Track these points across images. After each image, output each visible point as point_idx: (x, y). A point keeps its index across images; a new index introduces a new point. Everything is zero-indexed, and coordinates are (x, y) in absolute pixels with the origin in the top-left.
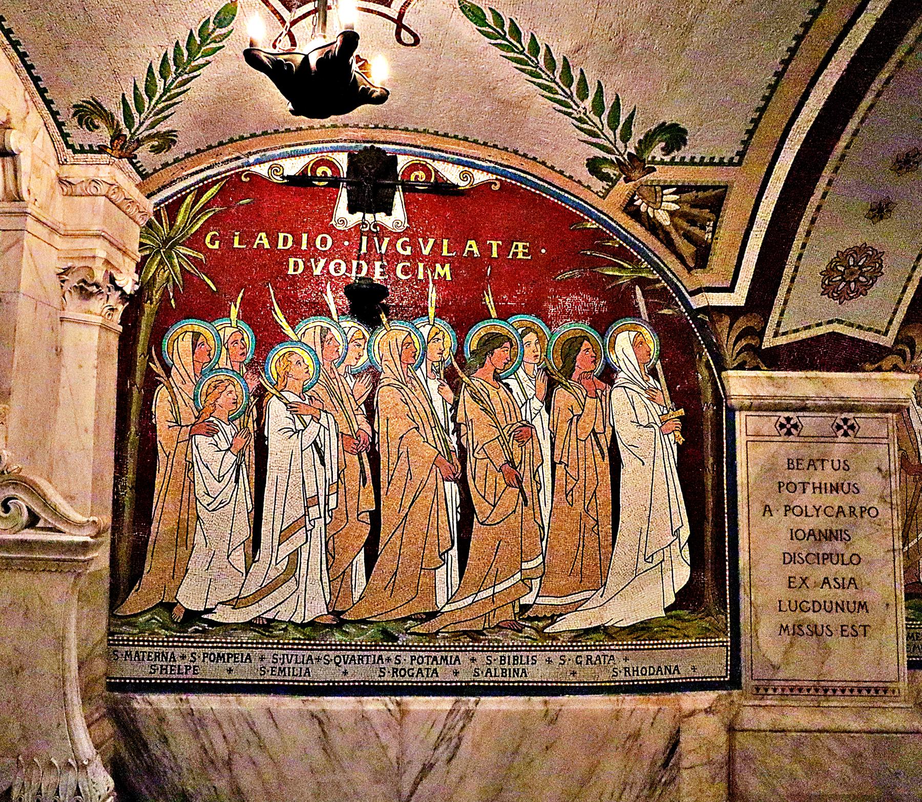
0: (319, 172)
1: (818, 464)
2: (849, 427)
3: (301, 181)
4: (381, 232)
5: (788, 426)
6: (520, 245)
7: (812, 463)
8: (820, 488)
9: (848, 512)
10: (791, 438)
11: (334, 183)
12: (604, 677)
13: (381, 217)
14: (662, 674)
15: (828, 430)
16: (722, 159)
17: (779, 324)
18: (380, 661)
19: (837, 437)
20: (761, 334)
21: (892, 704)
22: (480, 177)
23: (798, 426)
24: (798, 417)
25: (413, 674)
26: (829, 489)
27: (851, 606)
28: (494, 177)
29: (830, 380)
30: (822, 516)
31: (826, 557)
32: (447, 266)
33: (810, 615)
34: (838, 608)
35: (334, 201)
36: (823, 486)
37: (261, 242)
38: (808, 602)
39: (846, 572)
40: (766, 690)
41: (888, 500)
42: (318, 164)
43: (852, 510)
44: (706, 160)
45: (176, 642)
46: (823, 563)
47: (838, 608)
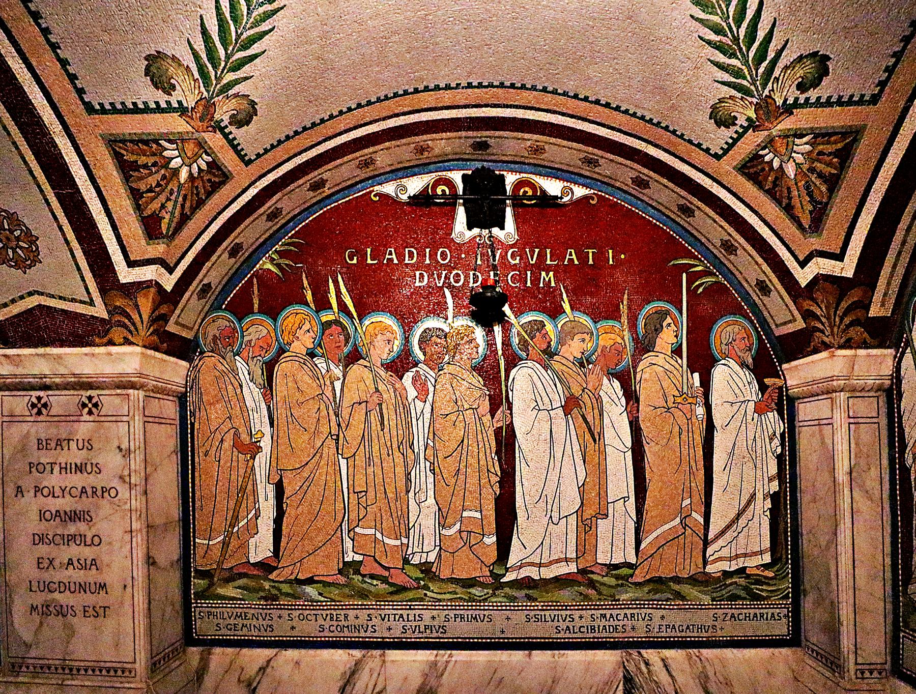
1: (65, 444)
4: (494, 244)
5: (39, 406)
7: (59, 443)
8: (66, 468)
9: (91, 493)
10: (41, 418)
13: (496, 231)
15: (73, 409)
17: (81, 302)
21: (127, 685)
23: (98, 405)
24: (47, 396)
25: (683, 630)
26: (73, 470)
27: (93, 587)
28: (592, 191)
29: (59, 357)
30: (67, 496)
31: (70, 538)
32: (551, 274)
33: (56, 595)
34: (81, 590)
35: (452, 217)
36: (68, 467)
37: (390, 257)
38: (55, 583)
39: (88, 553)
40: (21, 667)
41: (127, 479)
42: (437, 183)
43: (94, 490)
46: (68, 545)
47: (81, 590)
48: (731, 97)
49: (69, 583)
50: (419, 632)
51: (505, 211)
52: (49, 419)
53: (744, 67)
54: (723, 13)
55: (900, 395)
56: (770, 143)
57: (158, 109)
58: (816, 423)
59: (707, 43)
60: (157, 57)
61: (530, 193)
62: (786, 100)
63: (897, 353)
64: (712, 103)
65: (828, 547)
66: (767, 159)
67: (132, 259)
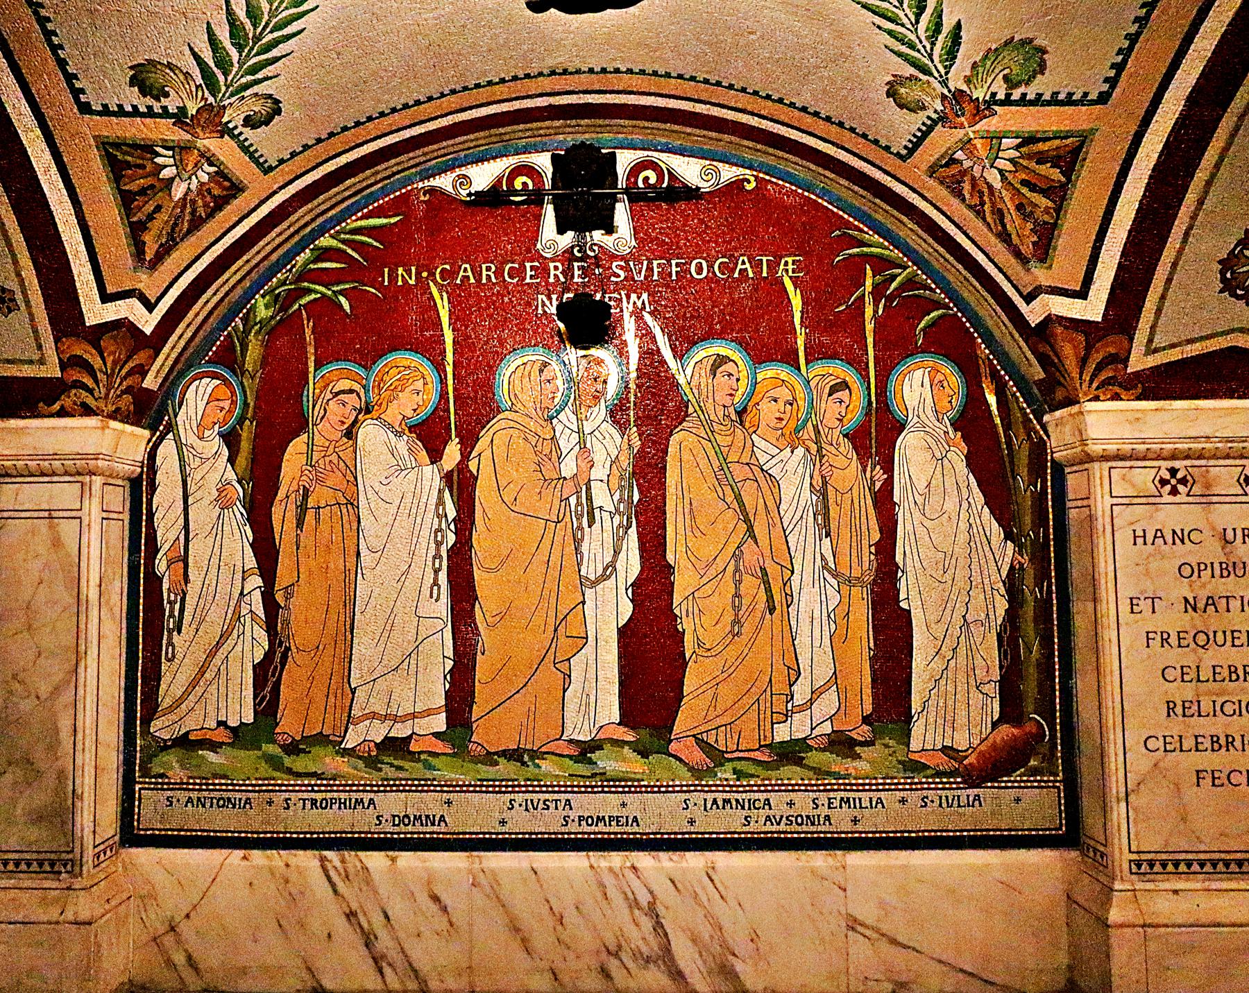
0: (518, 184)
2: (1168, 482)
5: (1173, 482)
6: (790, 260)
10: (1178, 499)
11: (536, 198)
12: (759, 826)
14: (422, 825)
18: (248, 806)
20: (1126, 361)
35: (538, 217)
44: (1047, 97)
45: (491, 786)
48: (187, 75)
52: (1191, 499)
53: (237, 65)
54: (277, 9)
55: (153, 488)
56: (181, 150)
58: (46, 514)
59: (227, 9)
62: (230, 122)
63: (153, 436)
64: (155, 57)
65: (56, 691)
66: (159, 160)
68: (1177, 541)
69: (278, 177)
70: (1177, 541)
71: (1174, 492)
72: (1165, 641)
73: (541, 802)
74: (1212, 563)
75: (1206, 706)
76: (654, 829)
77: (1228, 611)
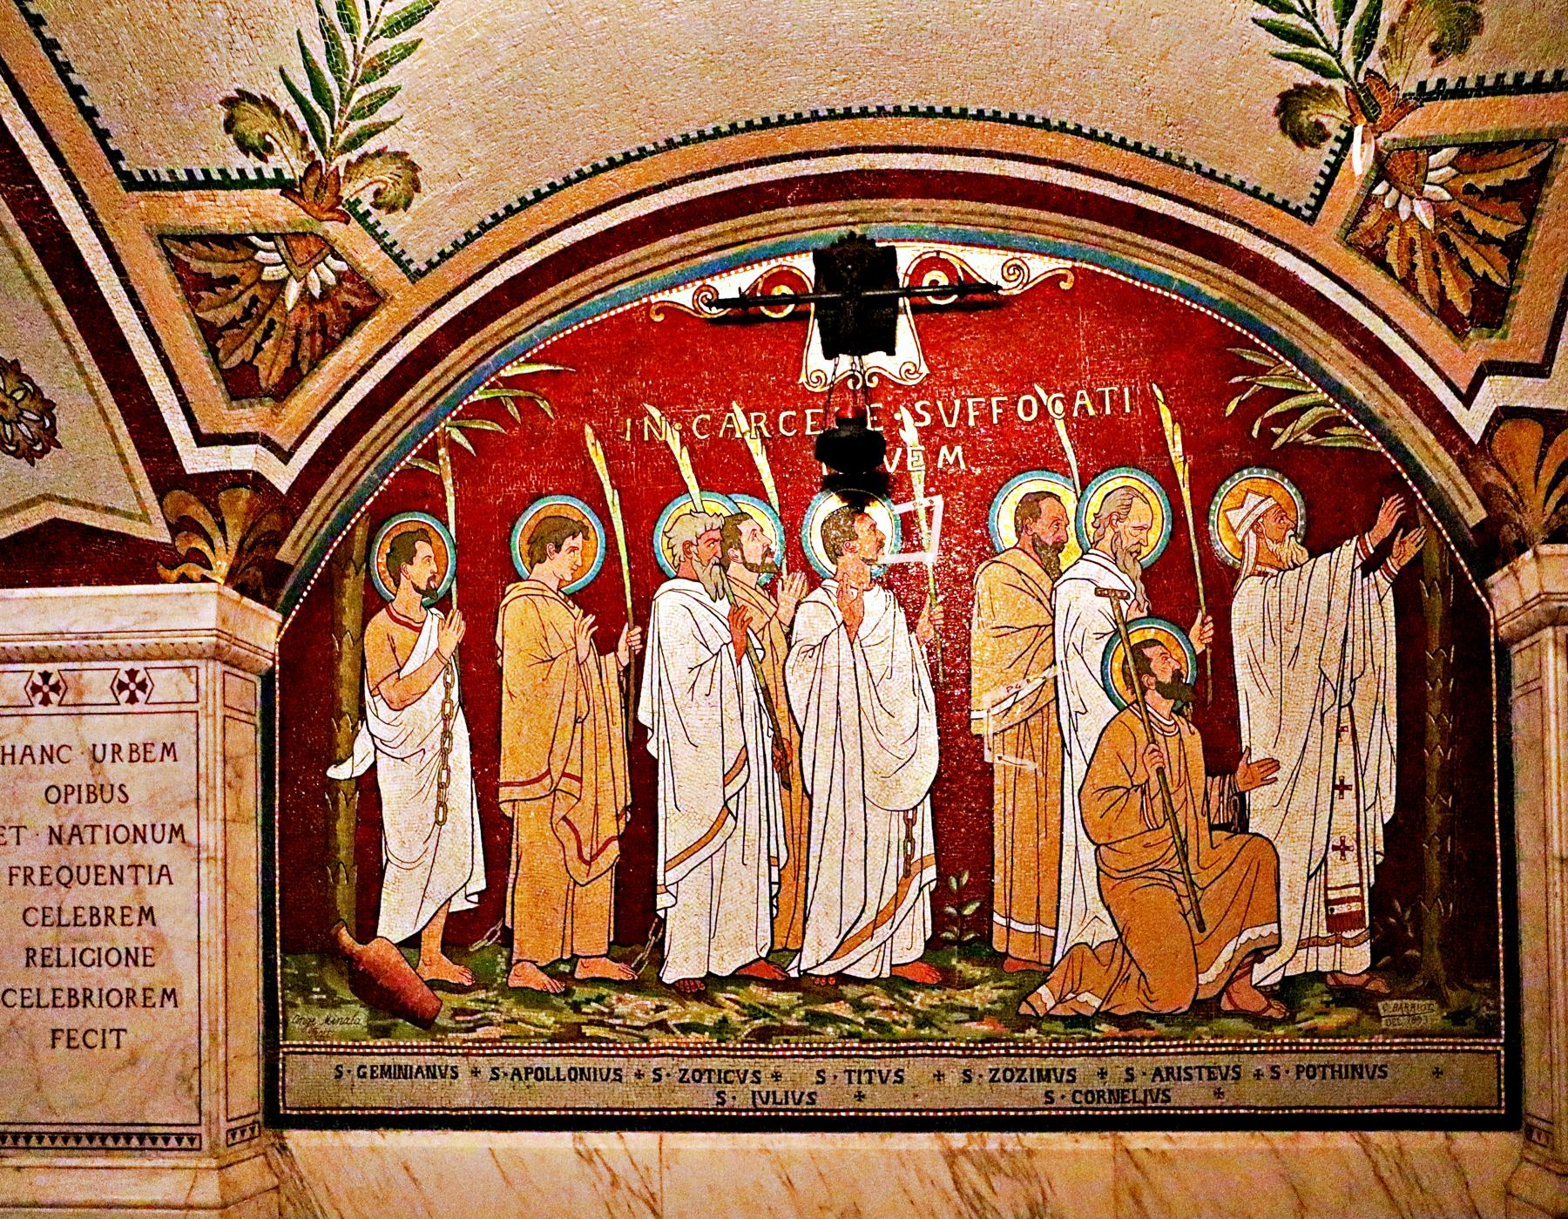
3: (745, 309)
10: (51, 709)
11: (800, 318)
13: (876, 359)
16: (1519, 77)
19: (32, 706)
22: (1039, 267)
24: (146, 669)
32: (958, 449)
49: (101, 1006)
50: (774, 1102)
51: (895, 324)
52: (62, 710)
57: (244, 183)
60: (236, 100)
61: (944, 280)
66: (260, 255)
67: (188, 472)
68: (46, 759)
69: (433, 286)
70: (46, 759)
71: (46, 701)
72: (28, 878)
73: (892, 1074)
74: (79, 786)
75: (66, 957)
76: (467, 1102)
77: (93, 842)
